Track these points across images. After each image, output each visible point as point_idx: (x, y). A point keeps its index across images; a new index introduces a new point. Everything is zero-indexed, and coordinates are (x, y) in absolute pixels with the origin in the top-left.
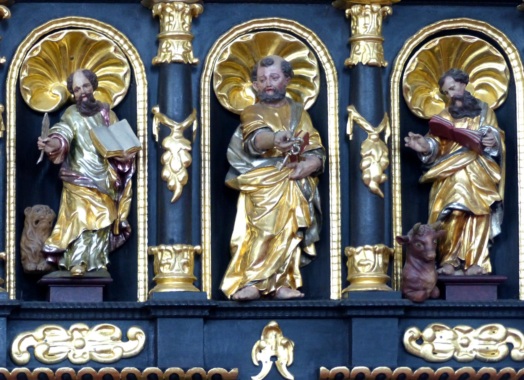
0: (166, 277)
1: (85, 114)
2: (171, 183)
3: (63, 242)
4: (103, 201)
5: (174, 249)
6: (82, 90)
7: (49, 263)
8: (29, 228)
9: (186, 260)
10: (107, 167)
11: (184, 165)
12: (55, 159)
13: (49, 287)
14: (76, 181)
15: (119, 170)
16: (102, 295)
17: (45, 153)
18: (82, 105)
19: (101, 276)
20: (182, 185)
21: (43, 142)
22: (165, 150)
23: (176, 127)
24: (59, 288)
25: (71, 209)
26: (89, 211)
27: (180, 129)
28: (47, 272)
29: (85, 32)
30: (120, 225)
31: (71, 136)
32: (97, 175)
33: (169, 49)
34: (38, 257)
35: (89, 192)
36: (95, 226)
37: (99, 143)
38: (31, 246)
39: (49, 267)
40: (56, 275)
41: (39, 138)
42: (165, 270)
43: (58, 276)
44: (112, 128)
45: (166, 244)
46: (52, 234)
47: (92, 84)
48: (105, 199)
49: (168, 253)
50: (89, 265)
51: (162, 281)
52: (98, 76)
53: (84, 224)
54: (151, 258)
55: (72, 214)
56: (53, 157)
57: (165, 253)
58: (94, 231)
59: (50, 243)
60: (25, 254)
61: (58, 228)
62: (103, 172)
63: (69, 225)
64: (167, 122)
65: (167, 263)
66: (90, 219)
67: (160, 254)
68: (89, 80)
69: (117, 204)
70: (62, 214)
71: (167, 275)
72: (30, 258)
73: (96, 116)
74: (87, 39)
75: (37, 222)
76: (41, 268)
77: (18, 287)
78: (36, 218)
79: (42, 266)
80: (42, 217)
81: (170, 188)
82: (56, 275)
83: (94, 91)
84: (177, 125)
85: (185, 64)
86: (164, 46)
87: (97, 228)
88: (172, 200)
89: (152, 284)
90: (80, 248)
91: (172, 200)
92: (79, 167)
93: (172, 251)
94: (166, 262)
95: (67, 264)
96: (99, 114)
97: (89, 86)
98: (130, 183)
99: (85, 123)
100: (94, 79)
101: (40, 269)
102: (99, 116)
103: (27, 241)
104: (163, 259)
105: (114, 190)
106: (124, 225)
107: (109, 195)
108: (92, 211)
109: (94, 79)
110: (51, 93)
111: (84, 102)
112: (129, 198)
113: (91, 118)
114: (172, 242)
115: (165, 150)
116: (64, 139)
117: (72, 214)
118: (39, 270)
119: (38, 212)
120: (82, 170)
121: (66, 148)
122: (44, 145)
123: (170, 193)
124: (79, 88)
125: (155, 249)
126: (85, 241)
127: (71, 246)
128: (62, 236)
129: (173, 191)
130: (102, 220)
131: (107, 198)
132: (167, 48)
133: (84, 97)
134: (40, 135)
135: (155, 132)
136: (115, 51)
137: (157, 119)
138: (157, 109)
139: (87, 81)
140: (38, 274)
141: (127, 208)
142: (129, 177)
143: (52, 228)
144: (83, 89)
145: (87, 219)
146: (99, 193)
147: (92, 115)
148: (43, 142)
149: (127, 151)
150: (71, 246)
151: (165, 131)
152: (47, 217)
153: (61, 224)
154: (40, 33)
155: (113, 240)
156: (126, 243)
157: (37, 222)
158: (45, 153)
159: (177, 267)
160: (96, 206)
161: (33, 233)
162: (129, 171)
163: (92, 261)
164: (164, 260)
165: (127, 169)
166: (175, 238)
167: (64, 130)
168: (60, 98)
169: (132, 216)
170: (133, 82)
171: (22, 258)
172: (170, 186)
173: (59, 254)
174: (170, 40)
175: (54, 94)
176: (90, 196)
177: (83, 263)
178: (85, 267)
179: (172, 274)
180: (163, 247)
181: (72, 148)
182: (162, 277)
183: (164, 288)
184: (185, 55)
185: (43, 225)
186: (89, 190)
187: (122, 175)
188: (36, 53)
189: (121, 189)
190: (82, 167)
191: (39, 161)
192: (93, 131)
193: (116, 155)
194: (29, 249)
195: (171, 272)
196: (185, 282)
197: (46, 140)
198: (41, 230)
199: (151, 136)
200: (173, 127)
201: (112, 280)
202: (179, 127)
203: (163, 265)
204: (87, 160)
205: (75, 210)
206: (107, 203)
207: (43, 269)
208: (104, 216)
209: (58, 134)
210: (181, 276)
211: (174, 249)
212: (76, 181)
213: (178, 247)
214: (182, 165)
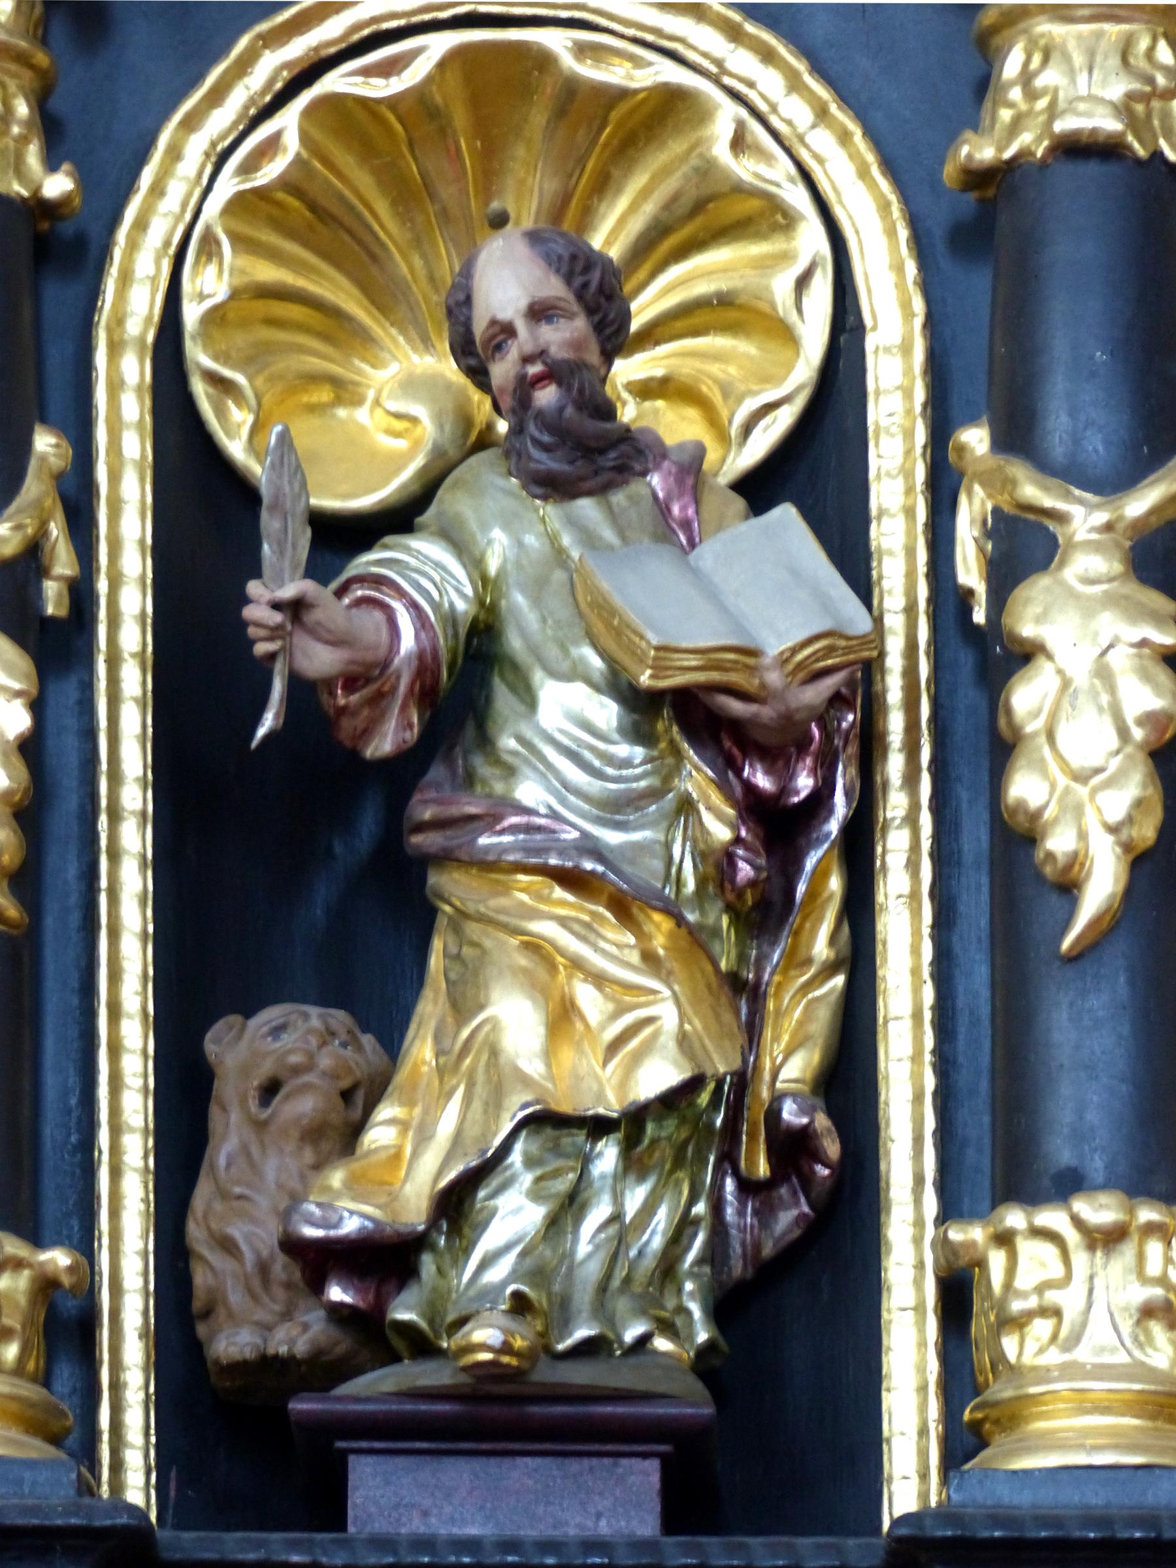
0: (1033, 1390)
1: (553, 487)
2: (1059, 843)
3: (408, 1188)
4: (649, 958)
5: (1077, 1222)
6: (525, 338)
7: (336, 1311)
8: (229, 1135)
9: (1159, 1292)
10: (677, 768)
11: (1138, 734)
12: (367, 733)
13: (344, 1454)
14: (484, 840)
15: (750, 788)
16: (656, 1505)
17: (299, 686)
18: (532, 428)
19: (642, 1386)
20: (1127, 847)
21: (276, 606)
22: (1025, 655)
23: (1084, 518)
24: (401, 1461)
25: (464, 1002)
26: (562, 1018)
27: (1109, 527)
28: (323, 1371)
29: (555, 40)
30: (773, 1114)
31: (461, 606)
32: (615, 809)
33: (1039, 82)
34: (280, 1293)
35: (563, 903)
36: (600, 1097)
37: (613, 612)
38: (237, 1232)
39: (343, 1343)
40: (376, 1386)
41: (254, 588)
42: (1026, 1348)
43: (388, 1386)
44: (707, 554)
45: (1032, 1199)
46: (359, 1152)
47: (590, 311)
48: (659, 944)
49: (1049, 1250)
50: (564, 1316)
51: (1011, 1416)
52: (615, 253)
53: (525, 1080)
54: (957, 1294)
55: (465, 1033)
56: (360, 722)
57: (1026, 1247)
58: (599, 1127)
59: (338, 1195)
60: (211, 1280)
61: (392, 1122)
62: (654, 794)
63: (450, 1095)
64: (1033, 491)
65: (1044, 1311)
66: (567, 1056)
67: (997, 1260)
68: (568, 279)
69: (745, 996)
70: (421, 1051)
71: (1042, 1374)
72: (235, 1297)
73: (618, 498)
74: (572, 88)
75: (270, 1090)
76: (292, 1342)
77: (168, 1458)
78: (266, 1069)
79: (299, 1335)
80: (295, 1059)
81: (1048, 870)
82: (376, 1386)
83: (608, 358)
84: (1091, 508)
85: (1138, 161)
86: (1012, 67)
87: (611, 1106)
88: (1066, 944)
89: (962, 1443)
90: (513, 1215)
91: (1066, 944)
92: (510, 772)
93: (1072, 1237)
94: (1032, 1303)
95: (433, 1312)
96: (636, 487)
97: (571, 316)
98: (835, 884)
99: (553, 539)
100: (596, 276)
101: (283, 1350)
102: (634, 500)
103: (218, 1206)
104: (1020, 1283)
105: (729, 908)
106: (790, 1113)
107: (696, 940)
108: (583, 1018)
109: (596, 276)
110: (379, 412)
111: (540, 415)
112: (830, 969)
113: (586, 507)
114: (1068, 1185)
115: (1025, 655)
116: (414, 606)
117: (465, 1033)
118: (276, 1357)
119: (274, 1040)
120: (529, 792)
121: (425, 664)
122: (277, 618)
123: (1054, 899)
124: (508, 330)
125: (974, 1234)
126: (538, 1180)
127: (457, 1204)
128: (409, 1152)
129: (1068, 888)
130: (637, 1058)
131: (671, 936)
132: (1026, 78)
133: (539, 380)
134: (256, 572)
135: (970, 572)
136: (739, 143)
137: (977, 488)
138: (976, 439)
139: (555, 288)
140: (272, 1374)
141: (822, 1021)
142: (819, 842)
143: (357, 1129)
144: (532, 333)
145: (549, 1054)
146: (623, 908)
147: (601, 491)
148: (276, 606)
149: (783, 660)
150: (457, 1204)
151: (1022, 548)
152: (325, 1061)
153: (410, 1103)
154: (298, 48)
155: (741, 1213)
156: (815, 1231)
157: (270, 1090)
158: (299, 686)
159: (1099, 1333)
160: (599, 980)
161: (248, 1155)
162: (820, 800)
163: (583, 1297)
164: (1023, 1295)
165: (805, 783)
166: (1096, 1166)
167: (428, 576)
168: (428, 429)
169: (848, 1075)
170: (851, 319)
171: (197, 1305)
172: (1050, 856)
173: (386, 1258)
174: (1046, 28)
175: (398, 416)
176: (563, 922)
177: (517, 1296)
178: (539, 1326)
179: (1070, 1370)
180: (1015, 1218)
181: (469, 677)
182: (1008, 1393)
183: (1029, 1450)
184: (1140, 108)
185: (302, 1106)
186: (559, 892)
187: (779, 827)
188: (271, 171)
189: (767, 913)
190: (526, 770)
191: (261, 732)
192: (591, 563)
193: (715, 676)
194: (227, 1246)
195: (1067, 1357)
196: (1153, 1417)
197: (288, 591)
198: (295, 1134)
199: (948, 600)
200: (1061, 518)
201: (708, 1410)
202: (1101, 517)
203: (1019, 1323)
204: (563, 734)
205: (481, 1007)
206: (676, 966)
207: (301, 1348)
208: (647, 1031)
209: (379, 581)
210: (1132, 1379)
211: (1077, 1222)
212: (484, 840)
213: (1100, 1210)
214: (1124, 733)
